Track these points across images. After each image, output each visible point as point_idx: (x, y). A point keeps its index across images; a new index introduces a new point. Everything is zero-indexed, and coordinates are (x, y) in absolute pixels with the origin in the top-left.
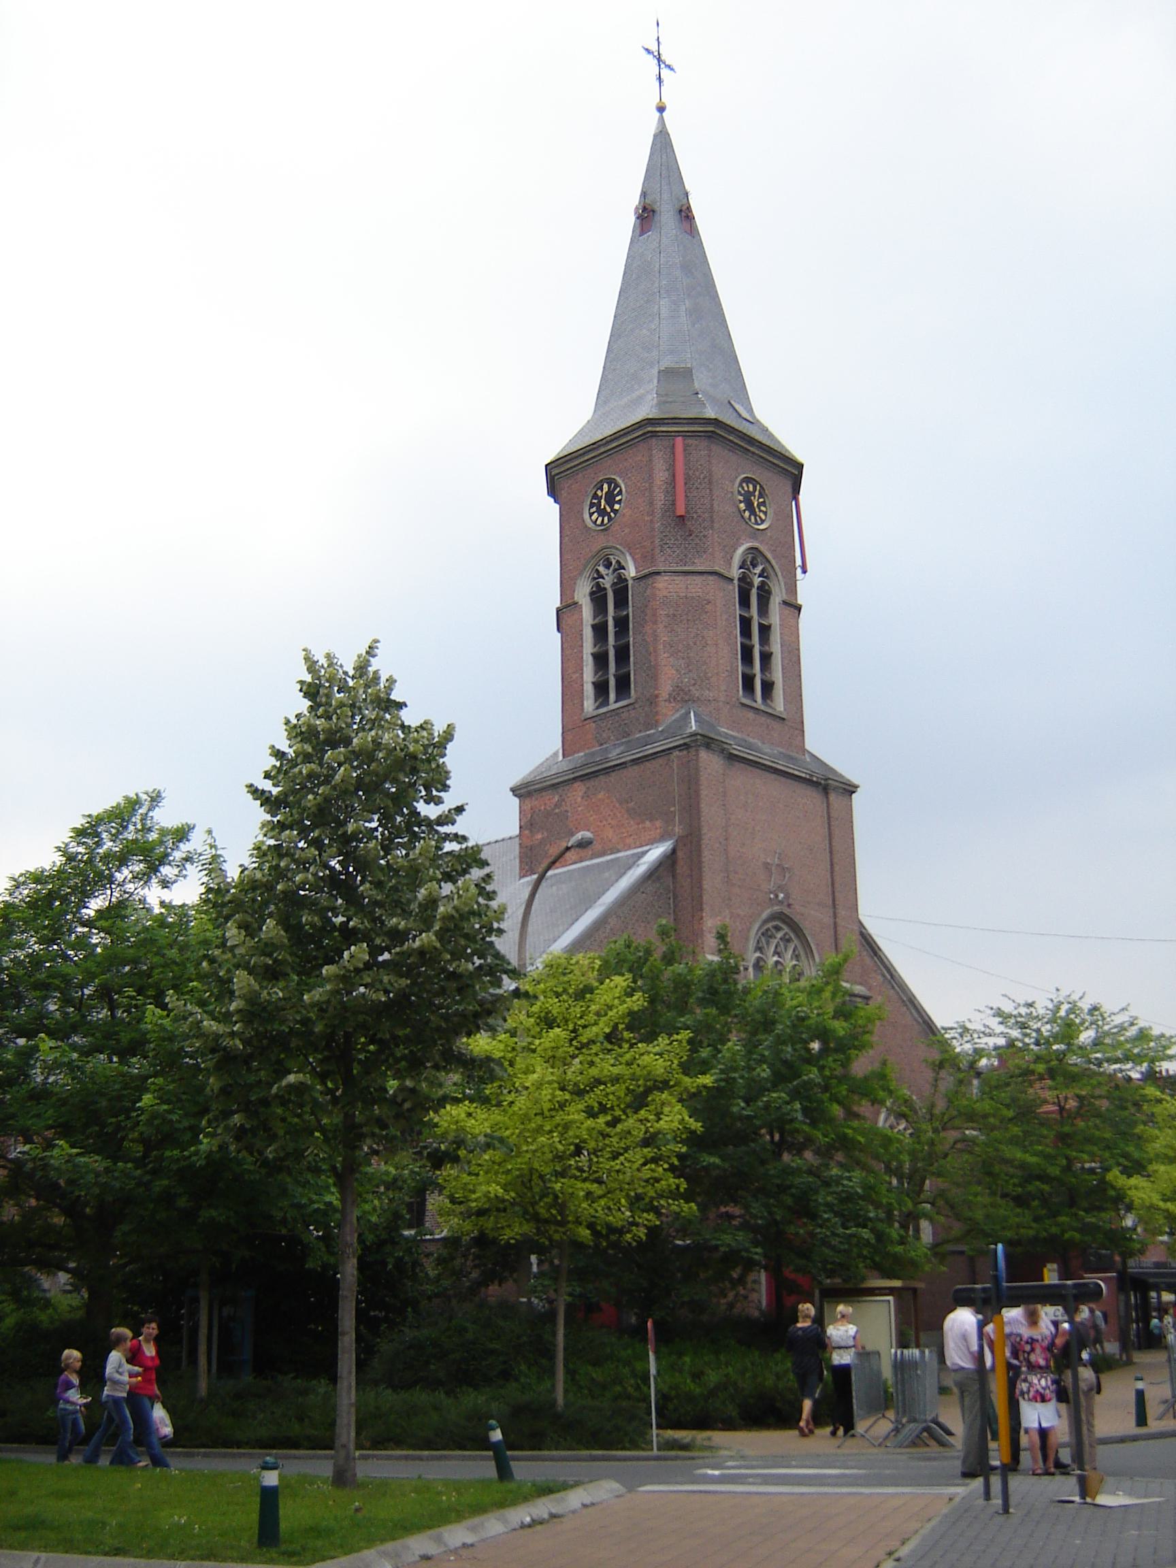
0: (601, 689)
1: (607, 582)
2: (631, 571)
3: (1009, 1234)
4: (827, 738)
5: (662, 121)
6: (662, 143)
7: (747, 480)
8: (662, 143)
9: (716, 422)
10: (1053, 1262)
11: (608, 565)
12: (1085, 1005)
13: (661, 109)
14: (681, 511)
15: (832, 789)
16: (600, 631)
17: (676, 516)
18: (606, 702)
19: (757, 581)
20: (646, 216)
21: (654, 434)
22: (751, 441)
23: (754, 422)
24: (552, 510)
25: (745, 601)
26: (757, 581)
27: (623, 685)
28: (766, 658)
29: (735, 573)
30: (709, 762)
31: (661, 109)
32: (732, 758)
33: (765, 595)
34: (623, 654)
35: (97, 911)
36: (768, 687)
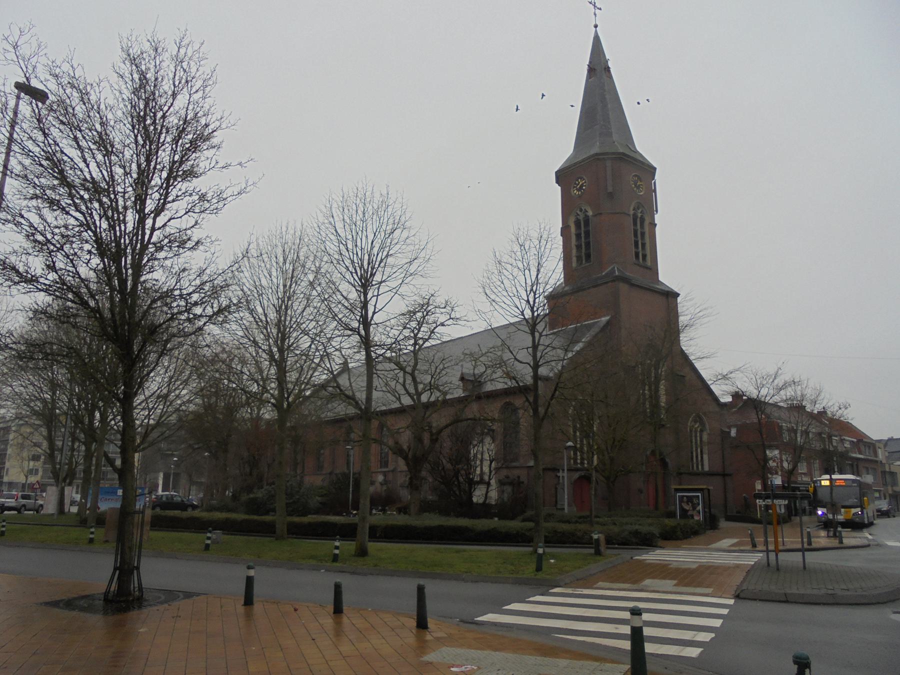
0: (579, 258)
1: (581, 217)
2: (590, 213)
3: (115, 497)
4: (667, 276)
5: (596, 31)
6: (597, 41)
7: (636, 176)
8: (597, 41)
9: (623, 154)
10: (477, 504)
11: (581, 210)
12: (440, 300)
13: (596, 26)
14: (610, 189)
15: (671, 296)
16: (578, 236)
17: (606, 193)
18: (581, 264)
19: (639, 215)
20: (591, 70)
21: (598, 159)
22: (636, 160)
23: (636, 152)
24: (558, 189)
25: (635, 224)
26: (639, 215)
27: (588, 256)
28: (643, 245)
29: (632, 212)
30: (623, 287)
31: (596, 26)
32: (633, 285)
33: (642, 220)
34: (588, 244)
35: (737, 396)
36: (644, 256)
